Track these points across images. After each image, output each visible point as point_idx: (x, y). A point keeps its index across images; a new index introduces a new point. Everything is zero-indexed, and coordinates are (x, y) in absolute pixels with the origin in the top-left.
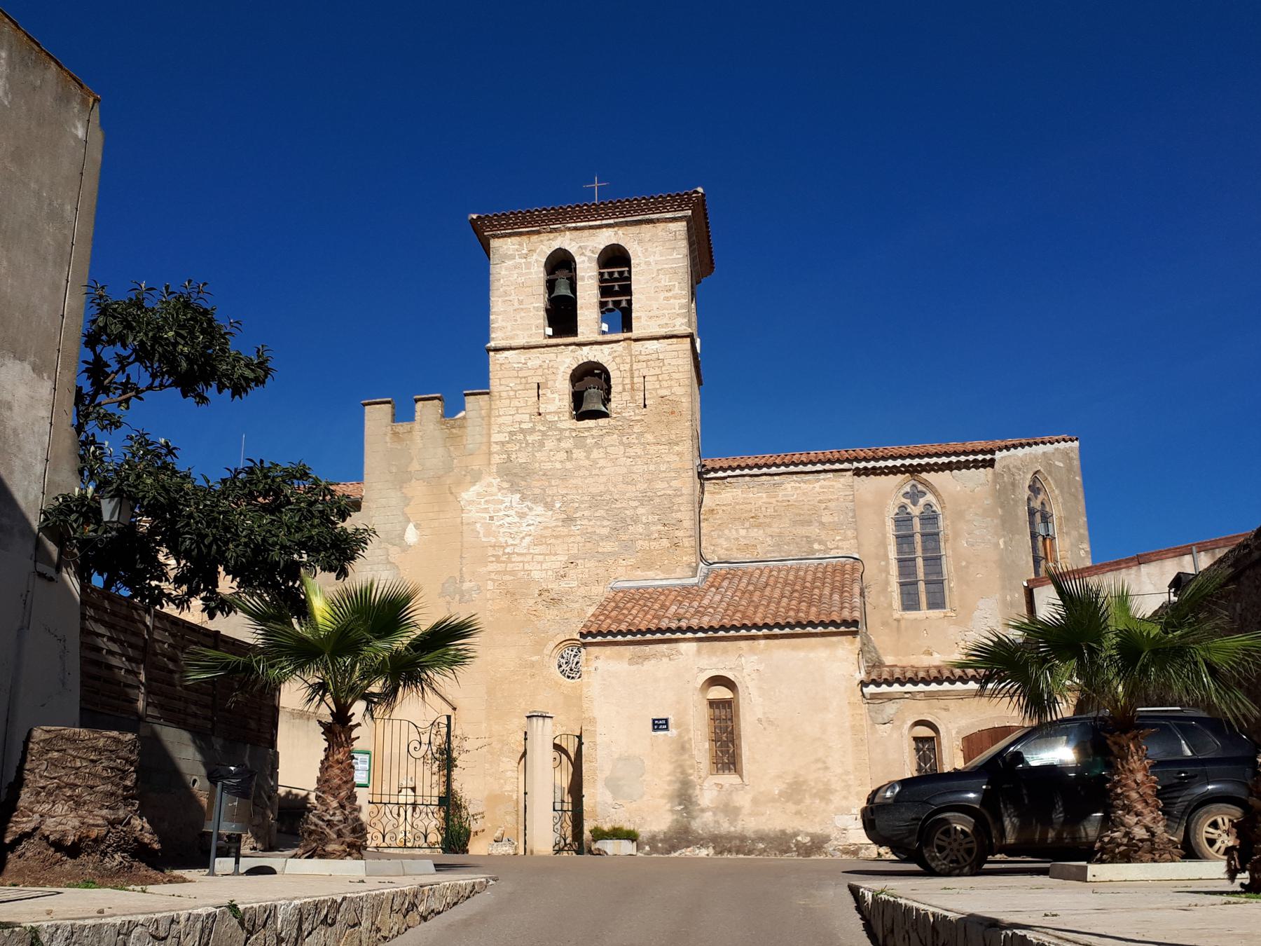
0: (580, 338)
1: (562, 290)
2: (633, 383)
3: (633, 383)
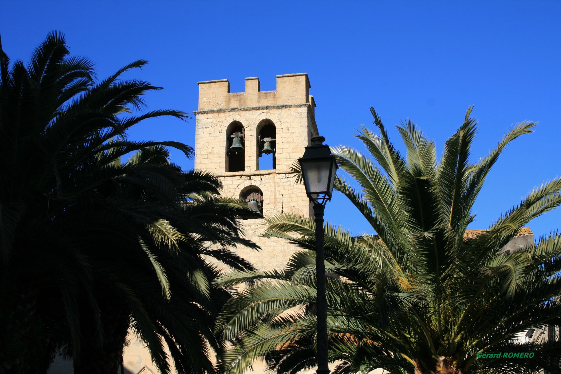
0: (247, 171)
1: (236, 144)
2: (275, 199)
3: (275, 199)
